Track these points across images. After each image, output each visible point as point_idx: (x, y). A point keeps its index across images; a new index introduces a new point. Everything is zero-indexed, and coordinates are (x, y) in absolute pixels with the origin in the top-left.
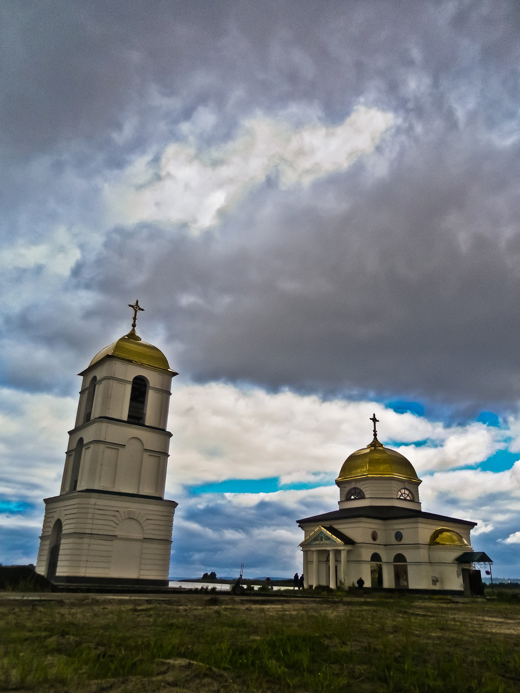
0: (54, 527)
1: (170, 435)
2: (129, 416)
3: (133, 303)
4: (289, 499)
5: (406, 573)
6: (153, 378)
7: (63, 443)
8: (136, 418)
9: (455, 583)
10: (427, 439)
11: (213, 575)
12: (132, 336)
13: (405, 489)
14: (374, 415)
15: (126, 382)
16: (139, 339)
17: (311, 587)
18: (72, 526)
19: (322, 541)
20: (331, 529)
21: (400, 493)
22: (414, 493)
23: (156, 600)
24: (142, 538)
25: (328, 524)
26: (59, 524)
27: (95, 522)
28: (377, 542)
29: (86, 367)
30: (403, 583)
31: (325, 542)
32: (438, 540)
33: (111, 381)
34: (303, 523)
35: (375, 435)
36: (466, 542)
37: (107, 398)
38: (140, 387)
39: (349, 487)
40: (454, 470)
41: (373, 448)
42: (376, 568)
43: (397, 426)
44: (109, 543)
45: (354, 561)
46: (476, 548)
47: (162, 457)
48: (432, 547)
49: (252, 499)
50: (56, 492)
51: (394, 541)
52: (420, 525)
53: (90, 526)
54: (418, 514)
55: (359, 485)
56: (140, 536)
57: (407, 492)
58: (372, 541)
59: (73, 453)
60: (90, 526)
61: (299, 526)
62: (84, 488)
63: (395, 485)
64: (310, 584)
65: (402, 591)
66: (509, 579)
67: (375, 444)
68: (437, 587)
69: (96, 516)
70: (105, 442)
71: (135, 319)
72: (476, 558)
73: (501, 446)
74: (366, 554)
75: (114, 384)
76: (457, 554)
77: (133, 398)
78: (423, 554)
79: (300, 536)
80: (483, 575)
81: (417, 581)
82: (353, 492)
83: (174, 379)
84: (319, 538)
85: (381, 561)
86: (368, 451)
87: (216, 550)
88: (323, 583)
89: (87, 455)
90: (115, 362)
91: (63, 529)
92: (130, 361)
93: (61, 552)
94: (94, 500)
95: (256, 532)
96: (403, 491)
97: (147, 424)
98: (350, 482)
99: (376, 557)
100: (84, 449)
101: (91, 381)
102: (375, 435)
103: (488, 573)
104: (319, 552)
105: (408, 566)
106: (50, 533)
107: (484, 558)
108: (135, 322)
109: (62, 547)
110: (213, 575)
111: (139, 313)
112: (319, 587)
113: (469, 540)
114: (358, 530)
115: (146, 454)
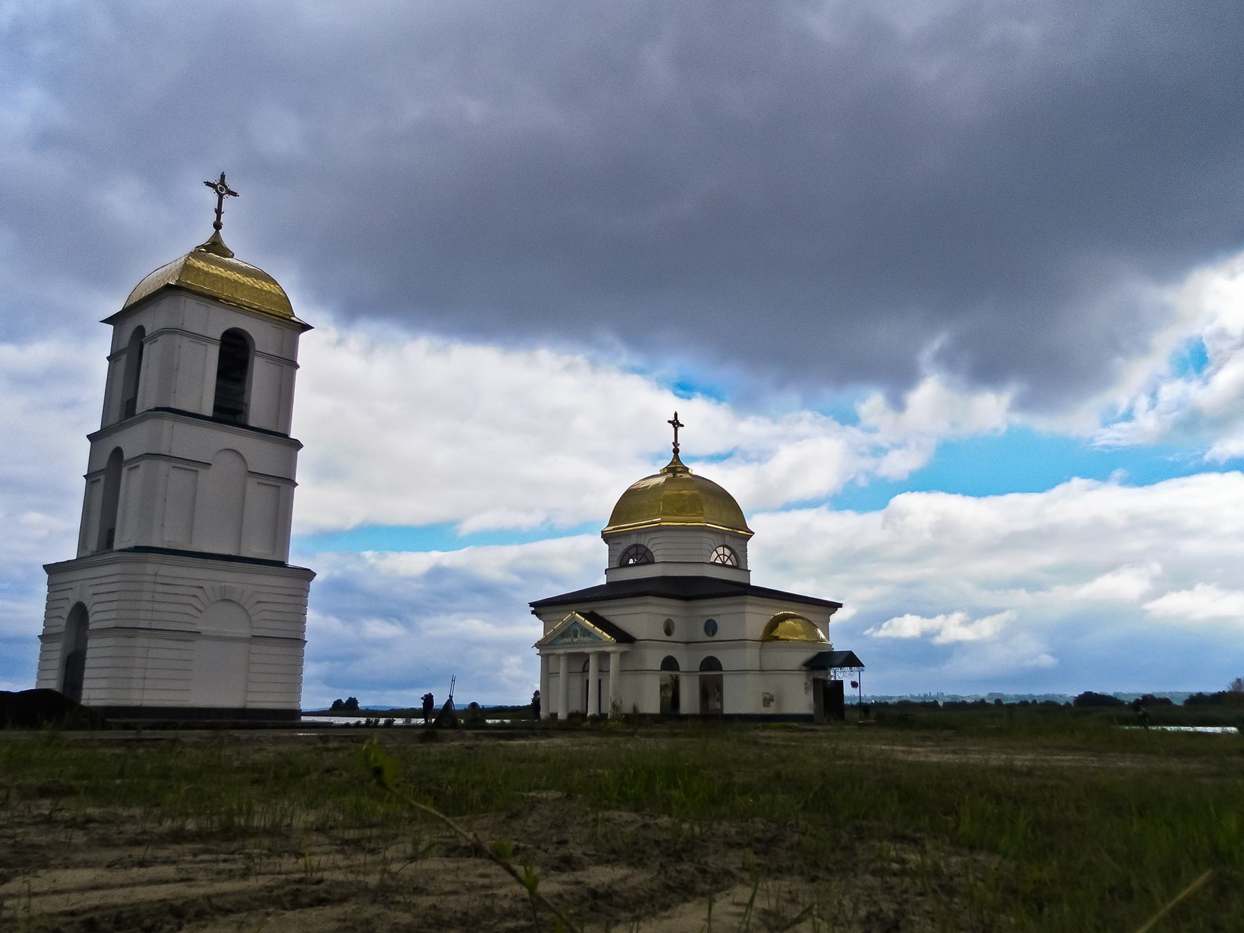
0: (69, 618)
1: (297, 445)
2: (216, 408)
3: (215, 180)
4: (491, 563)
5: (719, 688)
6: (262, 335)
7: (80, 456)
8: (230, 410)
9: (799, 701)
10: (736, 449)
11: (352, 702)
12: (215, 246)
13: (724, 546)
14: (676, 415)
15: (210, 340)
16: (226, 252)
17: (554, 716)
18: (113, 615)
19: (576, 636)
20: (592, 617)
21: (715, 554)
22: (740, 555)
23: (336, 737)
24: (249, 636)
25: (587, 608)
26: (80, 613)
27: (156, 606)
28: (673, 637)
29: (117, 307)
30: (714, 705)
31: (582, 639)
32: (776, 633)
33: (177, 338)
34: (541, 608)
36: (822, 636)
37: (169, 371)
38: (235, 354)
39: (626, 544)
40: (788, 507)
41: (670, 475)
42: (669, 681)
43: (712, 435)
44: (181, 645)
45: (631, 670)
46: (838, 644)
47: (283, 486)
48: (768, 644)
49: (416, 562)
50: (69, 552)
51: (701, 635)
52: (748, 608)
53: (149, 616)
54: (745, 590)
55: (642, 541)
56: (245, 632)
57: (727, 552)
58: (663, 636)
59: (102, 478)
60: (149, 616)
61: (533, 612)
62: (132, 544)
63: (708, 539)
64: (552, 710)
65: (712, 718)
66: (873, 697)
67: (676, 468)
68: (770, 710)
70: (169, 458)
71: (219, 212)
72: (839, 661)
73: (868, 463)
74: (653, 659)
75: (185, 342)
76: (808, 655)
77: (222, 374)
78: (750, 657)
79: (536, 629)
80: (848, 691)
81: (740, 698)
82: (633, 552)
83: (303, 337)
85: (677, 669)
86: (662, 480)
87: (354, 657)
88: (576, 706)
89: (132, 483)
90: (183, 299)
91: (91, 620)
92: (215, 299)
93: (89, 663)
94: (153, 567)
95: (425, 623)
96: (720, 550)
97: (251, 424)
98: (627, 534)
99: (669, 664)
100: (125, 471)
101: (133, 334)
103: (854, 685)
104: (570, 656)
105: (725, 679)
106: (62, 629)
107: (850, 660)
108: (219, 218)
109: (89, 654)
110: (352, 702)
111: (227, 200)
112: (571, 716)
113: (827, 634)
114: (641, 619)
115: (252, 483)
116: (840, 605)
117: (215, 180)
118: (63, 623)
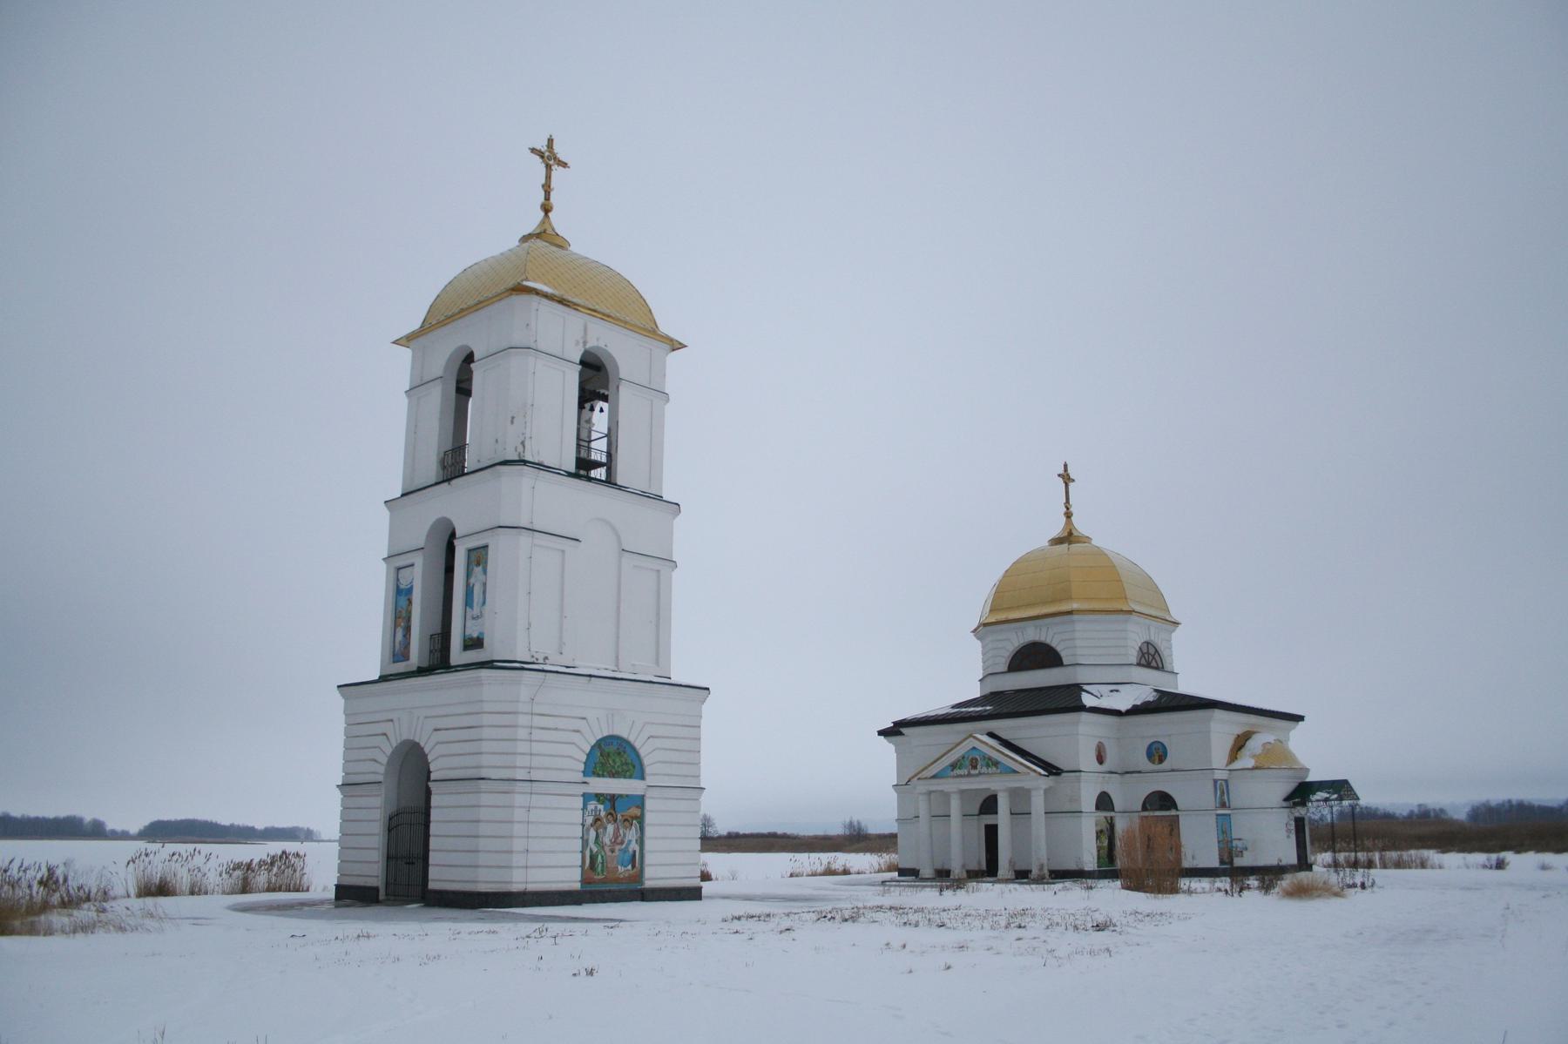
3: (542, 145)
12: (544, 234)
16: (560, 243)
19: (975, 767)
25: (1004, 727)
27: (537, 748)
31: (984, 770)
34: (1082, 708)
35: (1068, 515)
38: (595, 378)
51: (1143, 762)
69: (537, 734)
84: (967, 763)
99: (1104, 802)
102: (1068, 515)
108: (547, 198)
111: (557, 172)
116: (881, 733)
117: (542, 145)
118: (382, 769)
